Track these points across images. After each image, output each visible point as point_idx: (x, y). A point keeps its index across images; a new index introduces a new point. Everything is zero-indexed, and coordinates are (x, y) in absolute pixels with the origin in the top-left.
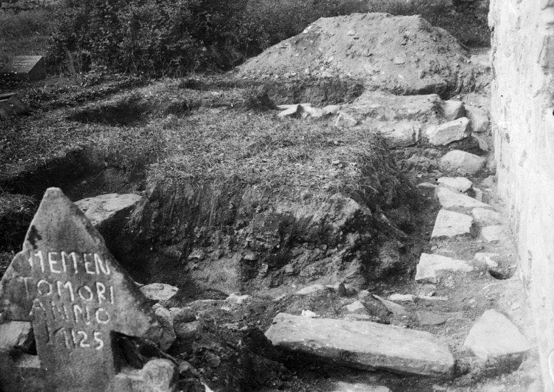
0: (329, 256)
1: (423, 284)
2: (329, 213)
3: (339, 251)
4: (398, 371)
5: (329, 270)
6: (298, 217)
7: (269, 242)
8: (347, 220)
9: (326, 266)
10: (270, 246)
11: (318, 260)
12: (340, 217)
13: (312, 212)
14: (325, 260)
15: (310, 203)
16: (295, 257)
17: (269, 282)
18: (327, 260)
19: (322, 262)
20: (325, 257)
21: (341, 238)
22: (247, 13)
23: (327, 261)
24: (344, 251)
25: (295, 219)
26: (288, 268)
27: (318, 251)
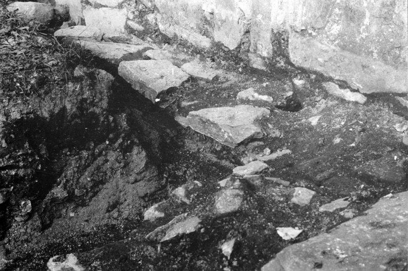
0: (100, 154)
1: (247, 144)
2: (85, 96)
3: (112, 141)
4: (226, 213)
5: (109, 174)
6: (46, 115)
7: (24, 167)
8: (108, 96)
9: (104, 169)
10: (29, 171)
11: (89, 166)
12: (99, 96)
13: (61, 103)
14: (97, 162)
15: (50, 91)
16: (59, 175)
17: (38, 223)
18: (100, 161)
19: (94, 166)
20: (95, 159)
21: (113, 125)
22: (250, 209)
23: (101, 162)
24: (120, 141)
25: (44, 119)
26: (58, 192)
27: (85, 154)
